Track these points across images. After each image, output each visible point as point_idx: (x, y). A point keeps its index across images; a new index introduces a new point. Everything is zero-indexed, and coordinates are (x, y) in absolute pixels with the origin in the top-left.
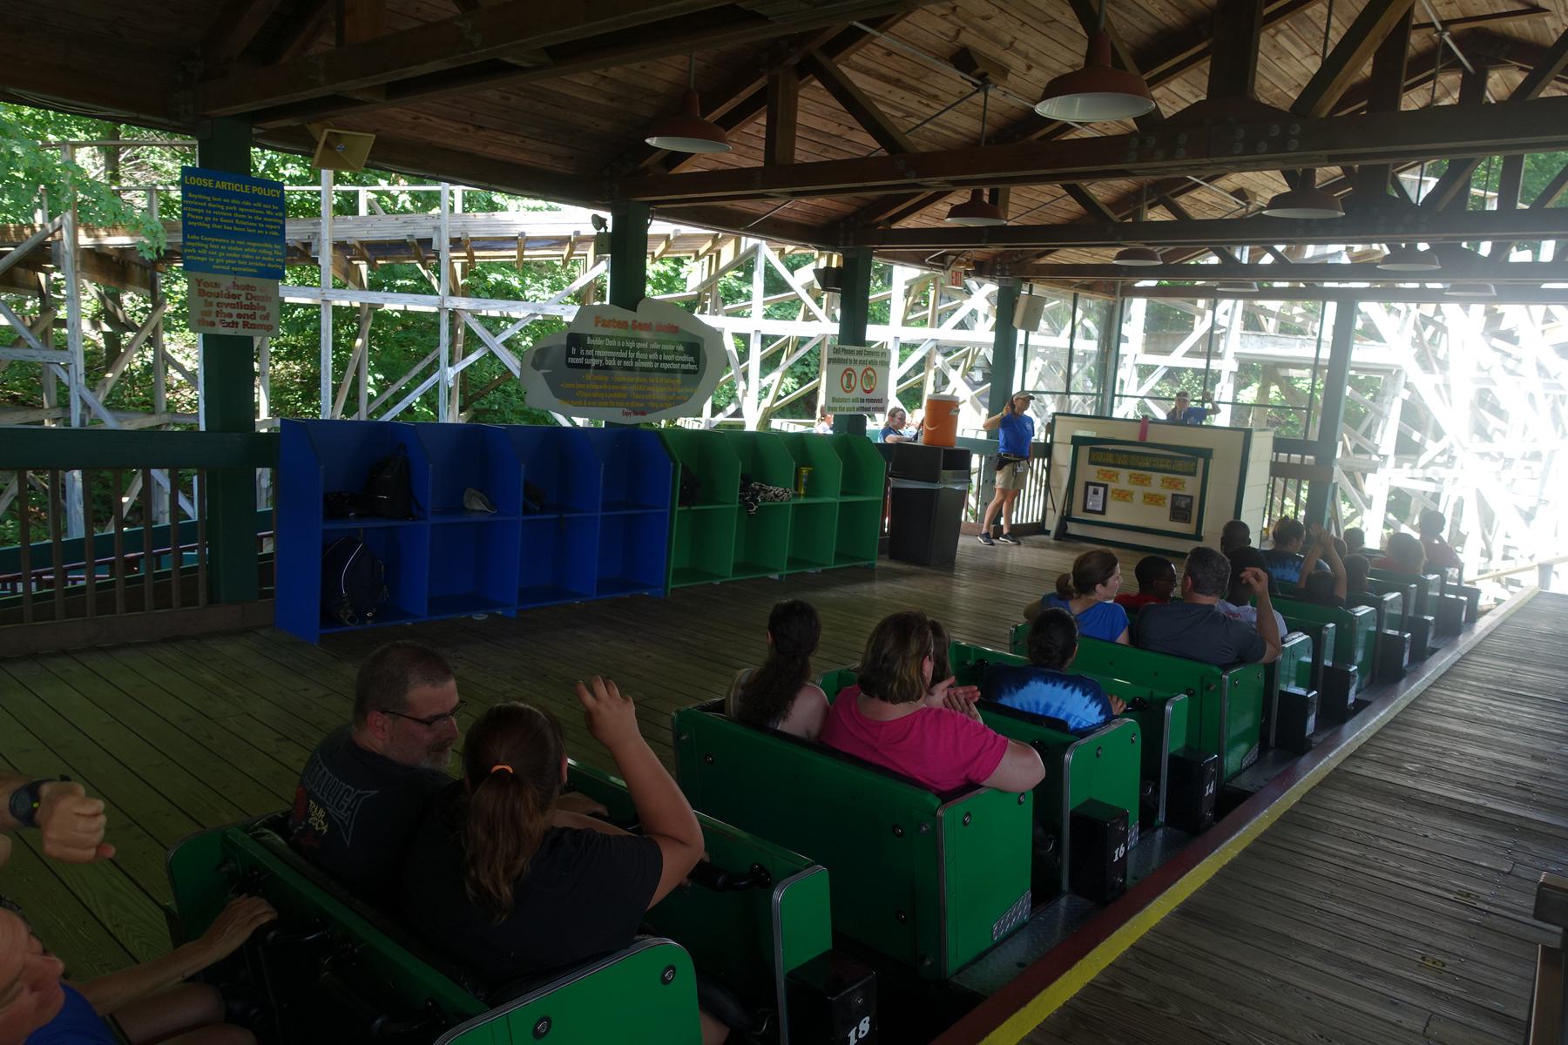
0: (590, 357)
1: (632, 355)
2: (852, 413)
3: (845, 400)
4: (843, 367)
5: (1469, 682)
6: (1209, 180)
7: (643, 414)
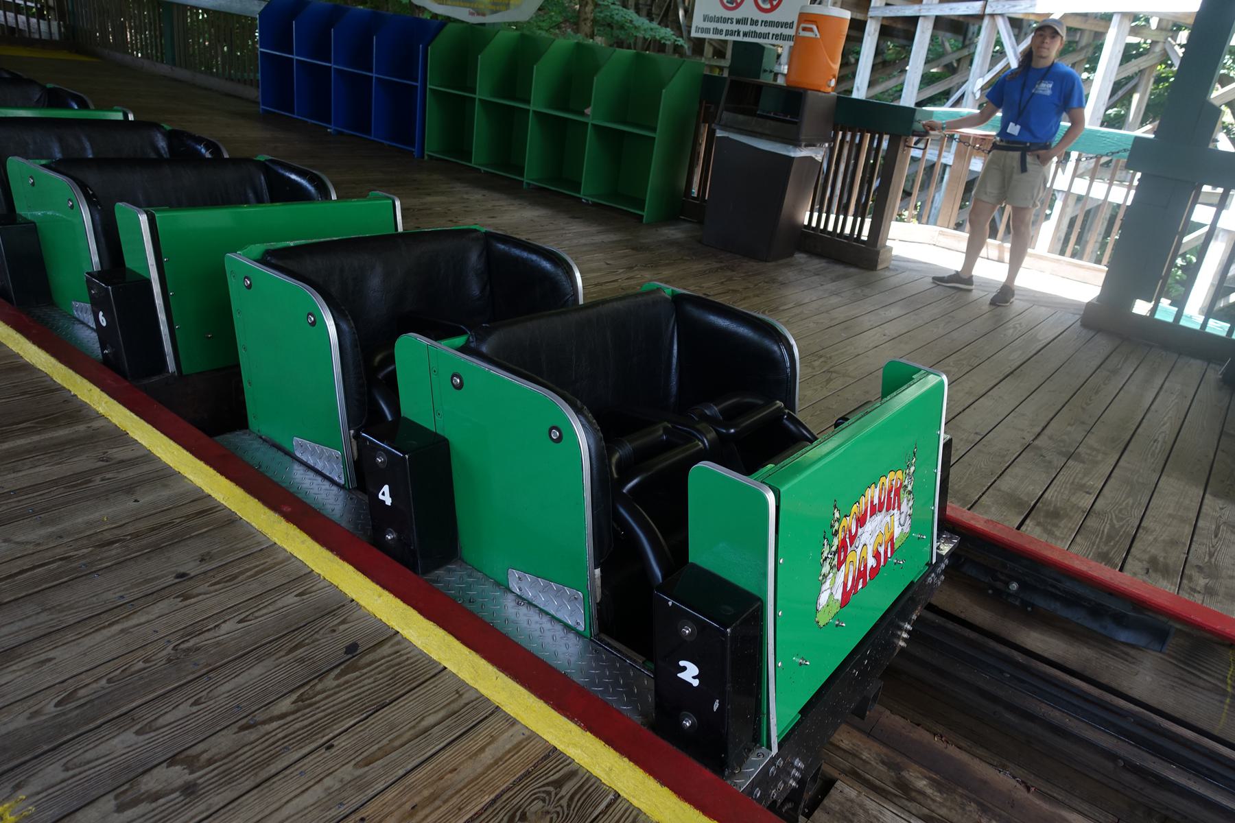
3: (725, 20)
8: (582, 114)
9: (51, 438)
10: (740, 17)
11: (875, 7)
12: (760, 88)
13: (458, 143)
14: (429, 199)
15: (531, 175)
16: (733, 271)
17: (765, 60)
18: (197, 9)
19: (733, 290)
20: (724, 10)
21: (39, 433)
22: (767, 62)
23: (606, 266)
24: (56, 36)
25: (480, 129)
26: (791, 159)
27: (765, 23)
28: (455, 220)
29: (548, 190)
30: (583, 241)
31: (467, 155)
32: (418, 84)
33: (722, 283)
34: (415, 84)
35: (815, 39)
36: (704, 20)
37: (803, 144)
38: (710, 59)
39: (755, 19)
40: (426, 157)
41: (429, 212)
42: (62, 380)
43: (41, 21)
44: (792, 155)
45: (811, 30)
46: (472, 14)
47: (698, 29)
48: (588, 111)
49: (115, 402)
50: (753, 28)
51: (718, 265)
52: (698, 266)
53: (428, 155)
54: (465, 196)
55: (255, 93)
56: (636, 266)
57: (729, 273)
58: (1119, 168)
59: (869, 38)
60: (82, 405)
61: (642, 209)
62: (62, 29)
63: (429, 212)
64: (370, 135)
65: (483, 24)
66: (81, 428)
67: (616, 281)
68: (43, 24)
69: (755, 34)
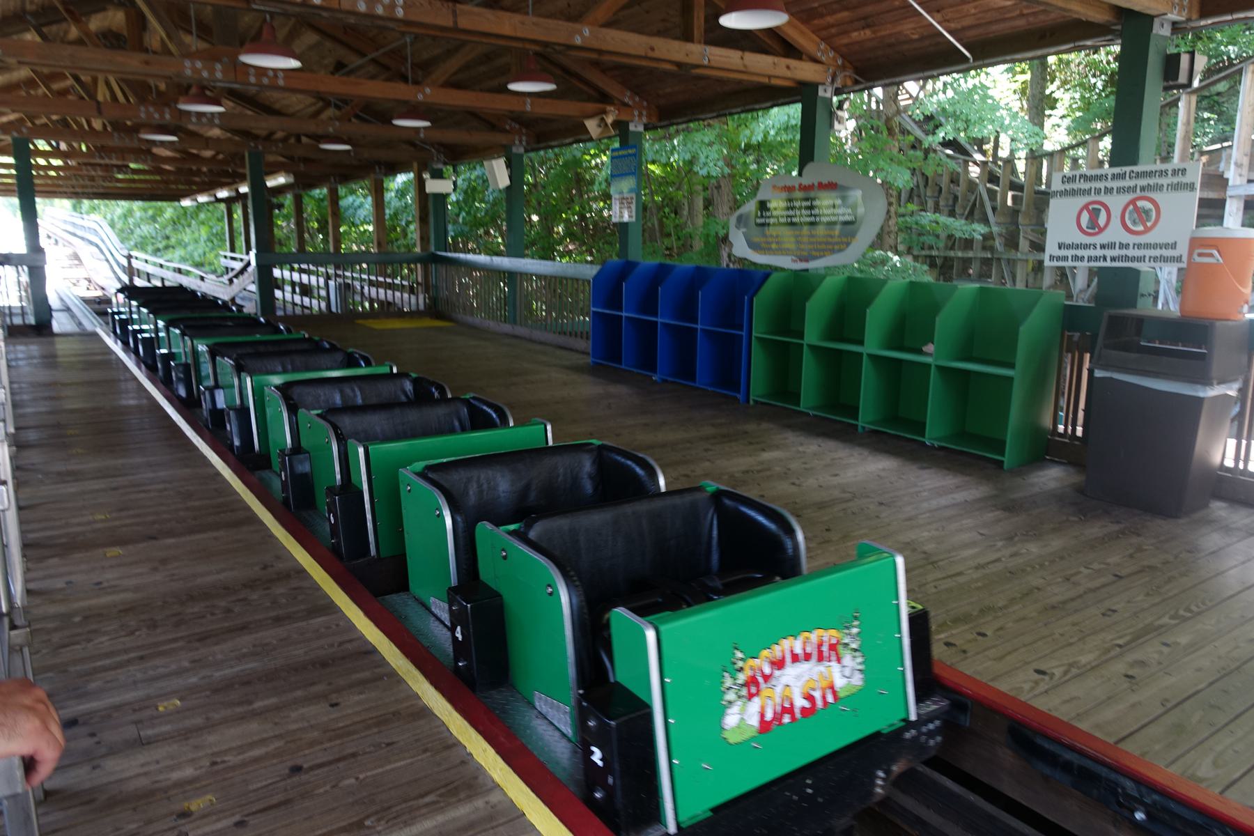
0: (769, 217)
1: (798, 213)
2: (1102, 264)
3: (1086, 247)
4: (1082, 201)
5: (161, 649)
6: (198, 36)
7: (807, 261)
8: (920, 352)
9: (454, 819)
10: (1105, 242)
11: (1234, 186)
12: (1140, 321)
13: (784, 386)
14: (766, 456)
15: (867, 416)
16: (1139, 535)
17: (1141, 284)
18: (532, 275)
19: (1149, 567)
20: (1084, 236)
21: (441, 810)
22: (1145, 286)
23: (980, 537)
24: (422, 307)
25: (810, 373)
26: (1200, 401)
27: (1139, 246)
28: (797, 482)
29: (889, 434)
30: (944, 501)
31: (795, 398)
32: (744, 334)
33: (1131, 556)
34: (740, 333)
35: (1218, 264)
36: (1060, 248)
37: (1215, 382)
38: (1026, 254)
39: (1124, 242)
40: (751, 402)
41: (768, 473)
42: (457, 732)
43: (412, 296)
44: (1201, 394)
45: (1211, 255)
46: (794, 261)
47: (1052, 258)
48: (929, 348)
49: (511, 770)
50: (1123, 252)
51: (1115, 527)
52: (1095, 530)
53: (754, 400)
54: (801, 449)
55: (585, 345)
56: (1016, 535)
57: (1135, 540)
58: (1199, 94)
59: (1231, 219)
60: (478, 769)
61: (1003, 455)
62: (427, 300)
63: (768, 473)
64: (695, 382)
65: (807, 270)
66: (479, 803)
67: (998, 560)
68: (413, 298)
69: (1127, 258)
